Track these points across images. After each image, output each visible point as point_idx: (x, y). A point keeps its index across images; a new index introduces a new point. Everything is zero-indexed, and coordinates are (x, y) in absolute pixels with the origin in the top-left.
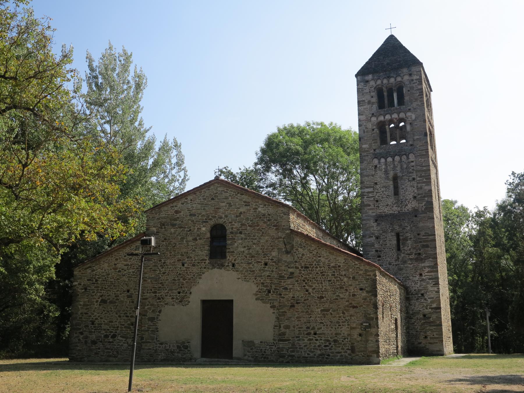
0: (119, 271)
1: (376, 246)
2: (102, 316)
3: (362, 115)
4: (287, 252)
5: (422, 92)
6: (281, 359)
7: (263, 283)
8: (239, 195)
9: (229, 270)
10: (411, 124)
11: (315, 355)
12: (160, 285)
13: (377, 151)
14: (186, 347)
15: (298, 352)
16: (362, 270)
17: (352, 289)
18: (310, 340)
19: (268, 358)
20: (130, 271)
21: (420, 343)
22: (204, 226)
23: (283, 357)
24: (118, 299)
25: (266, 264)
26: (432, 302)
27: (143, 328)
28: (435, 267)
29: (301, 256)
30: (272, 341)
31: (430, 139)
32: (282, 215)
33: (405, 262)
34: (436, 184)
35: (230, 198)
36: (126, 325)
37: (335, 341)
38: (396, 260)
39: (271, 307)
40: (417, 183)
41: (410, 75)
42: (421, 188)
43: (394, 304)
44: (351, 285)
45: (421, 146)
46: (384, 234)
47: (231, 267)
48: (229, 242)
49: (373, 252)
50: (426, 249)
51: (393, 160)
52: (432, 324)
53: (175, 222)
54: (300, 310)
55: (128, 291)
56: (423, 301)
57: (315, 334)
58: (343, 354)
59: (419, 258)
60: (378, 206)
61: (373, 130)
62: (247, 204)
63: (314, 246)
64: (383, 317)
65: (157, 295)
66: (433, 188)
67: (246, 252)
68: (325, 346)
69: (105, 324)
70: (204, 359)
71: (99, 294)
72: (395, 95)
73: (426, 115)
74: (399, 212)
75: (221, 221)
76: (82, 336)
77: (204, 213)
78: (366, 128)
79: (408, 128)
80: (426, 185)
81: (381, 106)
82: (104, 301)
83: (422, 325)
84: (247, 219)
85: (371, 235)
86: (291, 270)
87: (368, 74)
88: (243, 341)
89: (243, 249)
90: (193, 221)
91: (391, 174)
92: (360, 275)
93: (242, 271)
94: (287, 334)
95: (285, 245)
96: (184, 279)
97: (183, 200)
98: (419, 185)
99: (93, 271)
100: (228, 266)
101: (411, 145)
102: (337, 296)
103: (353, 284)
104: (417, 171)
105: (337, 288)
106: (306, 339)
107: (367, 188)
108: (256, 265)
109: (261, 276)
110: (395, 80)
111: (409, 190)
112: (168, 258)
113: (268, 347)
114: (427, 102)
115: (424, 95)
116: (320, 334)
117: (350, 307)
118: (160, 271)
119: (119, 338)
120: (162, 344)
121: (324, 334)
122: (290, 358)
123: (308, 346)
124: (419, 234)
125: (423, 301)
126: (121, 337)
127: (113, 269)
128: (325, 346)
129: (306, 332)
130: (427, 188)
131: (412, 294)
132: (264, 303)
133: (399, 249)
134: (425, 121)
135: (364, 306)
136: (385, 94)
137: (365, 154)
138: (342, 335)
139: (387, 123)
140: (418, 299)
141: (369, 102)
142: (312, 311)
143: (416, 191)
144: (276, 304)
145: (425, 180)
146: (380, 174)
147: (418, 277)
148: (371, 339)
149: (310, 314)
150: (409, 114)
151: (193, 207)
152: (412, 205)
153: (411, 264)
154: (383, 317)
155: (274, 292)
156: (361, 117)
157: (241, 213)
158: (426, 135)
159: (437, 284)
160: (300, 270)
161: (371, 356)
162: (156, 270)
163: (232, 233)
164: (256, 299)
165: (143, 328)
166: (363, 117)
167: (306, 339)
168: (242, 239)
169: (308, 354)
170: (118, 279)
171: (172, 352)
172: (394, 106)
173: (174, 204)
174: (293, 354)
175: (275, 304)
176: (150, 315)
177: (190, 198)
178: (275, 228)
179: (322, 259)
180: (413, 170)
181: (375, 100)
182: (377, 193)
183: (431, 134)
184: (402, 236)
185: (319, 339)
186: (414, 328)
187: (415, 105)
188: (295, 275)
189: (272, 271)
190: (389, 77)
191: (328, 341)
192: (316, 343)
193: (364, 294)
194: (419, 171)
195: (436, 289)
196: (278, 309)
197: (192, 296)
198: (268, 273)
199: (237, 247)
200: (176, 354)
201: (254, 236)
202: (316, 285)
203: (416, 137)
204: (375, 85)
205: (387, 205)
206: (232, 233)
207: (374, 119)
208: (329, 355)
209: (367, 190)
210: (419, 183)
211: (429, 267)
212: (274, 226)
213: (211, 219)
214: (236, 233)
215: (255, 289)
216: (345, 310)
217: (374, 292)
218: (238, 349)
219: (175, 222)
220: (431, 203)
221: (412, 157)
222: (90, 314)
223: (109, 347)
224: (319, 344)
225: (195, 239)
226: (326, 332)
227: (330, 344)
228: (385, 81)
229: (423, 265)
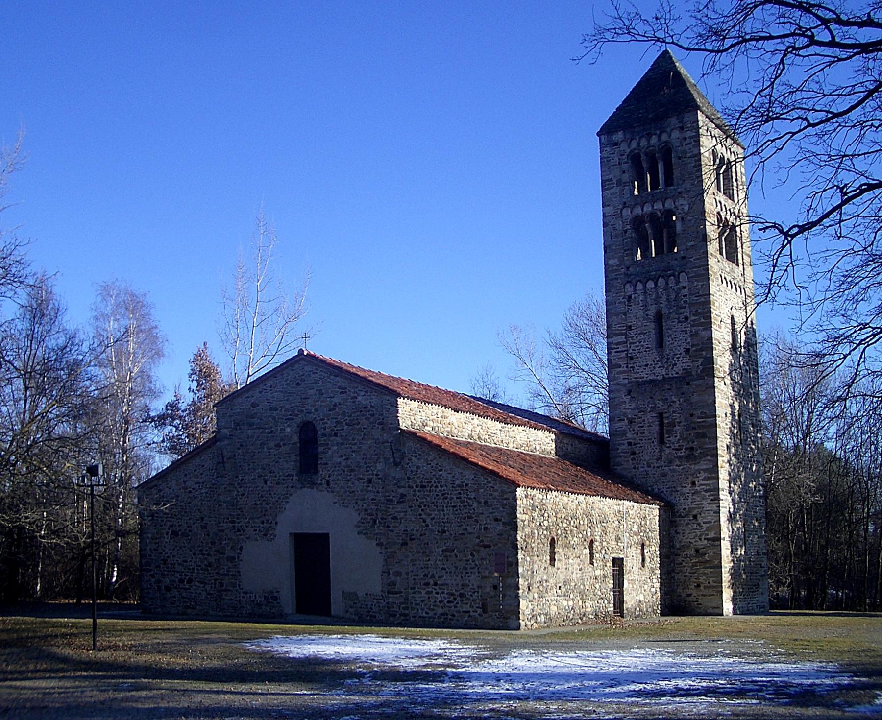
0: (190, 492)
1: (629, 435)
3: (609, 205)
4: (396, 464)
7: (366, 510)
8: (332, 377)
11: (435, 614)
14: (275, 598)
16: (496, 491)
18: (428, 593)
19: (375, 617)
21: (690, 595)
22: (288, 426)
24: (190, 531)
26: (708, 529)
27: (221, 572)
30: (380, 594)
32: (389, 406)
33: (670, 462)
37: (461, 595)
38: (658, 460)
40: (692, 326)
41: (682, 128)
44: (482, 514)
45: (698, 259)
47: (325, 486)
48: (321, 449)
50: (702, 440)
52: (707, 565)
53: (252, 420)
55: (202, 519)
56: (695, 527)
57: (436, 584)
58: (472, 614)
59: (691, 457)
61: (626, 232)
63: (433, 455)
65: (236, 525)
67: (344, 463)
68: (449, 602)
69: (179, 564)
71: (169, 523)
75: (310, 418)
76: (153, 580)
77: (287, 406)
78: (615, 229)
80: (704, 330)
82: (175, 533)
83: (693, 566)
85: (622, 417)
86: (401, 491)
88: (343, 592)
89: (339, 460)
90: (274, 418)
92: (495, 498)
94: (398, 584)
95: (393, 453)
96: (267, 504)
97: (262, 387)
99: (160, 491)
100: (321, 484)
103: (485, 512)
104: (691, 305)
105: (464, 518)
106: (423, 592)
108: (356, 482)
109: (364, 499)
110: (659, 139)
111: (678, 339)
116: (442, 585)
122: (403, 618)
123: (426, 602)
125: (695, 527)
127: (183, 488)
128: (449, 602)
131: (680, 516)
133: (662, 441)
135: (500, 545)
138: (471, 586)
140: (688, 524)
142: (431, 552)
144: (383, 540)
148: (508, 593)
151: (273, 397)
152: (682, 365)
153: (679, 466)
156: (607, 208)
157: (335, 405)
160: (415, 491)
161: (509, 618)
163: (324, 435)
164: (358, 533)
167: (423, 592)
169: (427, 613)
170: (189, 503)
171: (259, 605)
174: (406, 612)
176: (229, 553)
180: (685, 302)
182: (631, 343)
184: (668, 417)
185: (440, 591)
186: (681, 571)
189: (378, 492)
190: (649, 136)
191: (452, 594)
193: (500, 527)
195: (714, 507)
199: (332, 457)
201: (354, 440)
204: (628, 151)
206: (324, 435)
207: (626, 212)
208: (453, 615)
211: (705, 470)
212: (380, 424)
213: (297, 415)
214: (330, 436)
216: (475, 550)
218: (337, 605)
222: (160, 551)
223: (184, 594)
225: (278, 446)
226: (449, 582)
227: (455, 599)
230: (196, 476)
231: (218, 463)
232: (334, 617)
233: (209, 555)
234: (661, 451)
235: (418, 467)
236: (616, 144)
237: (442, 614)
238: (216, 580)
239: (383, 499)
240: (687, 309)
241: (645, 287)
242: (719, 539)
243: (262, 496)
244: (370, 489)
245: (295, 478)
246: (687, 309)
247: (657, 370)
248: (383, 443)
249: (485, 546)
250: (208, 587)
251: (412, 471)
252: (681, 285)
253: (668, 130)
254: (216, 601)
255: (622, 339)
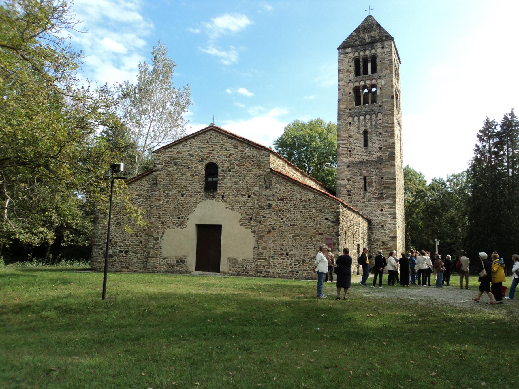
2: (118, 235)
5: (392, 62)
6: (259, 274)
7: (246, 212)
9: (219, 201)
10: (381, 88)
12: (164, 212)
13: (352, 111)
14: (183, 262)
15: (272, 268)
17: (318, 219)
18: (283, 259)
19: (248, 273)
20: (141, 200)
23: (261, 272)
25: (249, 196)
26: (389, 232)
28: (393, 205)
29: (278, 191)
31: (396, 103)
33: (369, 200)
34: (399, 139)
35: (222, 142)
36: (136, 243)
37: (303, 261)
38: (363, 198)
39: (252, 232)
42: (386, 141)
43: (357, 233)
44: (318, 216)
46: (354, 177)
49: (345, 192)
51: (365, 118)
53: (176, 161)
54: (276, 235)
56: (382, 231)
57: (287, 254)
59: (381, 197)
60: (351, 155)
61: (350, 93)
62: (236, 147)
64: (345, 243)
66: (396, 142)
68: (295, 265)
69: (120, 242)
70: (198, 272)
72: (369, 65)
73: (394, 81)
74: (367, 160)
75: (214, 161)
78: (344, 92)
79: (379, 92)
81: (357, 74)
84: (235, 160)
86: (269, 202)
87: (348, 47)
90: (191, 161)
91: (362, 129)
93: (229, 202)
96: (183, 208)
98: (385, 139)
101: (380, 106)
102: (307, 224)
104: (383, 127)
106: (279, 259)
107: (342, 140)
110: (370, 52)
111: (375, 142)
112: (171, 190)
113: (249, 264)
114: (395, 72)
115: (394, 65)
117: (317, 234)
118: (164, 200)
119: (131, 253)
120: (164, 259)
121: (294, 255)
122: (266, 273)
124: (382, 178)
126: (132, 252)
128: (295, 265)
129: (279, 253)
130: (391, 141)
131: (374, 225)
132: (246, 228)
133: (365, 190)
134: (392, 86)
136: (361, 64)
137: (342, 113)
139: (361, 88)
140: (378, 230)
141: (348, 71)
142: (285, 236)
143: (382, 143)
144: (256, 229)
145: (389, 135)
146: (353, 129)
147: (379, 212)
149: (284, 239)
150: (379, 81)
154: (345, 243)
155: (255, 220)
158: (392, 97)
159: (395, 218)
160: (277, 203)
162: (160, 200)
165: (149, 246)
166: (342, 83)
167: (279, 259)
168: (230, 176)
169: (281, 271)
171: (172, 266)
172: (368, 74)
173: (177, 146)
174: (269, 270)
175: (255, 229)
176: (155, 235)
177: (189, 141)
178: (257, 167)
179: (295, 193)
180: (380, 126)
181: (353, 68)
183: (397, 98)
185: (290, 258)
187: (385, 72)
188: (273, 206)
189: (254, 203)
190: (365, 50)
191: (297, 260)
192: (287, 262)
194: (385, 127)
196: (258, 234)
197: (189, 221)
198: (250, 204)
200: (175, 267)
202: (290, 215)
203: (384, 100)
205: (358, 154)
206: (222, 171)
207: (351, 84)
208: (298, 272)
209: (342, 142)
210: (385, 137)
211: (389, 204)
213: (205, 159)
215: (240, 216)
216: (313, 236)
217: (337, 222)
218: (224, 265)
219: (176, 161)
220: (393, 153)
221: (380, 116)
224: (290, 263)
225: (193, 175)
227: (299, 263)
228: (362, 53)
229: (384, 202)
230: (137, 191)
231: (153, 184)
232: (222, 273)
233: (141, 236)
234: (365, 194)
235: (280, 190)
236: (347, 53)
237: (290, 272)
238: (144, 251)
239: (257, 207)
240: (381, 130)
241: (359, 119)
242: (396, 237)
243: (180, 203)
244: (249, 201)
245: (202, 193)
246: (381, 130)
247: (364, 157)
248: (260, 176)
249: (320, 234)
250: (139, 256)
251: (276, 192)
252: (378, 118)
253: (376, 48)
254: (143, 263)
255: (346, 142)
